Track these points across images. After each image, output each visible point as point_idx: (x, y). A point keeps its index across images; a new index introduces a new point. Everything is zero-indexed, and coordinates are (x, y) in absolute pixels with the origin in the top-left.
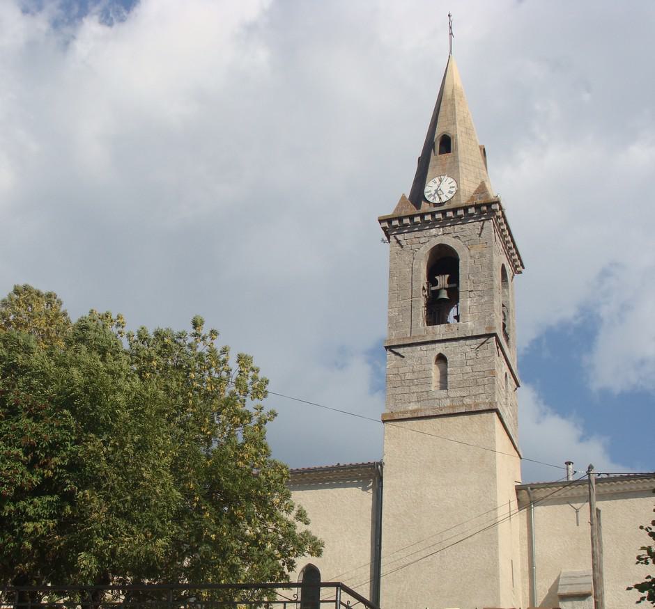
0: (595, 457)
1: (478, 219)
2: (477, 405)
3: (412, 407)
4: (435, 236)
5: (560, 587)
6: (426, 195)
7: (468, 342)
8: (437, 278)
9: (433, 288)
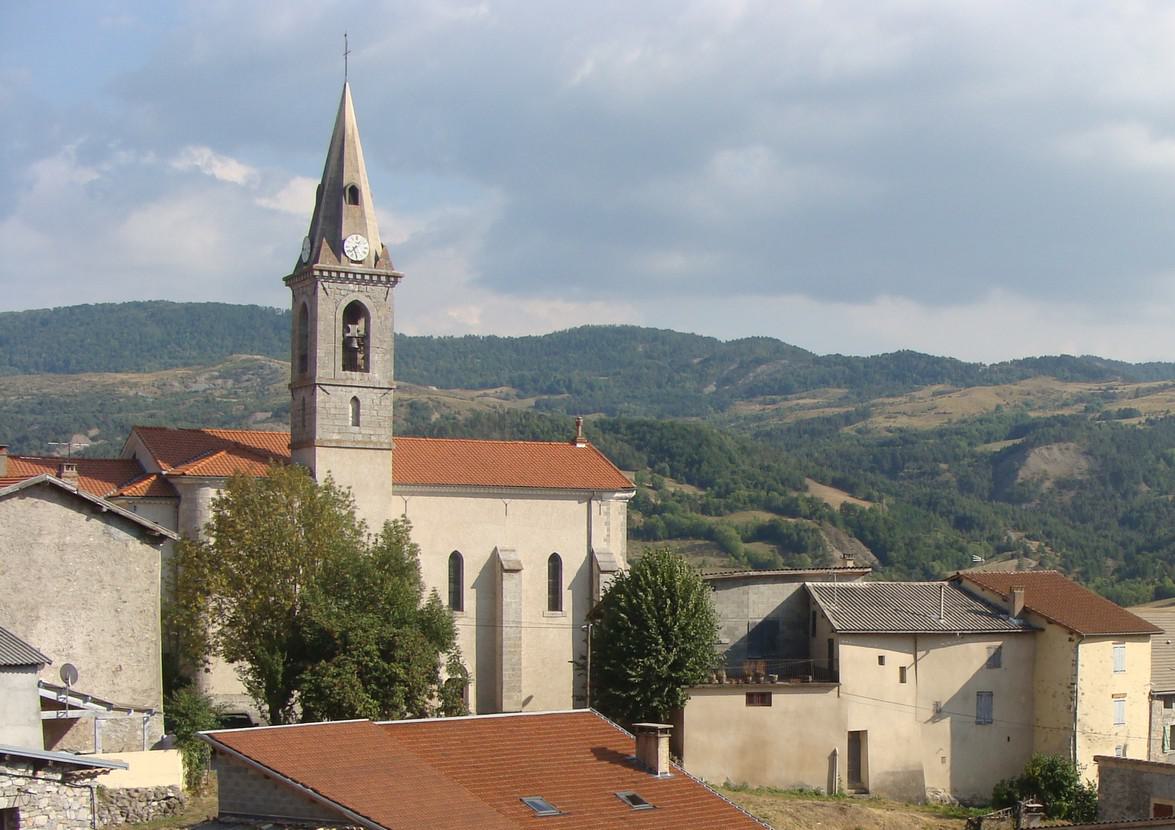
0: (342, 255)
1: (385, 284)
2: (381, 444)
3: (336, 437)
4: (353, 291)
5: (1152, 760)
6: (346, 250)
7: (376, 391)
8: (350, 326)
9: (348, 335)
